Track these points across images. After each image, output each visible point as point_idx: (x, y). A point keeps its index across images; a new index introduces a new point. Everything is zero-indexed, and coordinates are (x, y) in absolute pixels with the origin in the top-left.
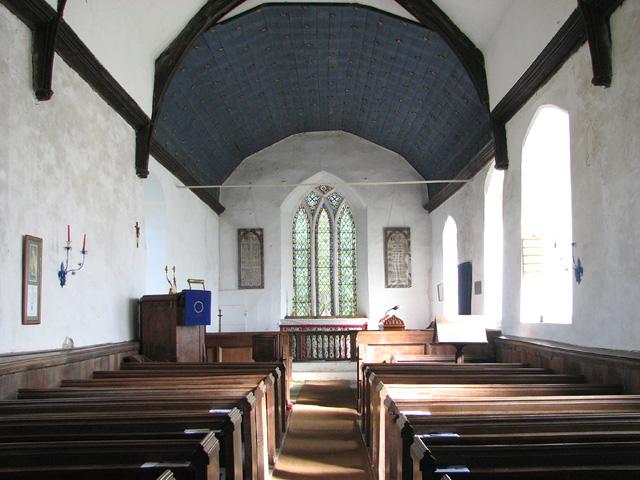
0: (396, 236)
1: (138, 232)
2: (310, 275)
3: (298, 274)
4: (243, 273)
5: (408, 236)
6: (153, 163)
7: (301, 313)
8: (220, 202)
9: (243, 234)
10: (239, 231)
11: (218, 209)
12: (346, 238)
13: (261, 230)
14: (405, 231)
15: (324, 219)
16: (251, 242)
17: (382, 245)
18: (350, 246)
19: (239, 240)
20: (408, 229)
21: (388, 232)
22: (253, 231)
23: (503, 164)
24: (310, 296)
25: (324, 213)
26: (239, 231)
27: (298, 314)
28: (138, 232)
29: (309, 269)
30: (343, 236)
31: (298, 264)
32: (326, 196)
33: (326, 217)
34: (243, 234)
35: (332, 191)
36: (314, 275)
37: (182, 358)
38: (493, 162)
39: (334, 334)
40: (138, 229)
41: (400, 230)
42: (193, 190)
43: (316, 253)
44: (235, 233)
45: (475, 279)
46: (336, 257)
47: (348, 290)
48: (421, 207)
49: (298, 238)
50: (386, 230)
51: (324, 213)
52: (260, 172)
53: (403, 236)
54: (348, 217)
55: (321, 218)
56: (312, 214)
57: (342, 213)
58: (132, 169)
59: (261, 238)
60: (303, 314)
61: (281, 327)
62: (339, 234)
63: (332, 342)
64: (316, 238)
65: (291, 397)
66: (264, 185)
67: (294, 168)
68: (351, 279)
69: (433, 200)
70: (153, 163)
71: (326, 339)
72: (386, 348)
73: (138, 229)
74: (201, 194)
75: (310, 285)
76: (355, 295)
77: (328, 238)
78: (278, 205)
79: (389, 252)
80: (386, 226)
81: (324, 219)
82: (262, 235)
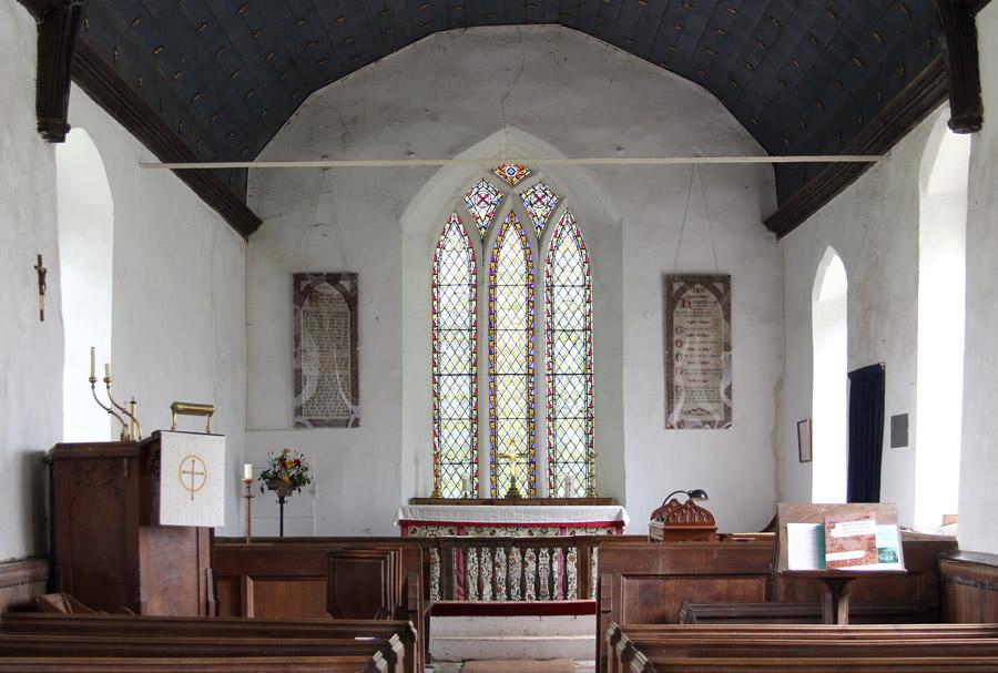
0: (694, 295)
1: (42, 282)
3: (444, 390)
6: (79, 101)
7: (451, 490)
11: (245, 222)
12: (570, 305)
14: (716, 285)
15: (511, 253)
16: (327, 305)
18: (577, 322)
20: (726, 279)
21: (676, 287)
22: (334, 279)
23: (968, 118)
24: (474, 447)
25: (512, 237)
27: (446, 494)
28: (42, 282)
30: (560, 296)
31: (447, 364)
32: (517, 190)
33: (518, 247)
34: (304, 288)
37: (154, 605)
38: (944, 112)
39: (537, 544)
40: (42, 275)
42: (179, 173)
45: (891, 409)
47: (570, 432)
49: (444, 300)
50: (669, 280)
51: (512, 237)
52: (348, 132)
54: (573, 248)
55: (506, 248)
57: (558, 236)
58: (29, 119)
59: (352, 301)
60: (457, 494)
61: (404, 524)
63: (532, 566)
66: (363, 161)
67: (434, 118)
68: (581, 404)
69: (790, 206)
70: (79, 101)
72: (670, 583)
73: (42, 275)
74: (202, 184)
75: (475, 420)
80: (669, 269)
81: (511, 253)
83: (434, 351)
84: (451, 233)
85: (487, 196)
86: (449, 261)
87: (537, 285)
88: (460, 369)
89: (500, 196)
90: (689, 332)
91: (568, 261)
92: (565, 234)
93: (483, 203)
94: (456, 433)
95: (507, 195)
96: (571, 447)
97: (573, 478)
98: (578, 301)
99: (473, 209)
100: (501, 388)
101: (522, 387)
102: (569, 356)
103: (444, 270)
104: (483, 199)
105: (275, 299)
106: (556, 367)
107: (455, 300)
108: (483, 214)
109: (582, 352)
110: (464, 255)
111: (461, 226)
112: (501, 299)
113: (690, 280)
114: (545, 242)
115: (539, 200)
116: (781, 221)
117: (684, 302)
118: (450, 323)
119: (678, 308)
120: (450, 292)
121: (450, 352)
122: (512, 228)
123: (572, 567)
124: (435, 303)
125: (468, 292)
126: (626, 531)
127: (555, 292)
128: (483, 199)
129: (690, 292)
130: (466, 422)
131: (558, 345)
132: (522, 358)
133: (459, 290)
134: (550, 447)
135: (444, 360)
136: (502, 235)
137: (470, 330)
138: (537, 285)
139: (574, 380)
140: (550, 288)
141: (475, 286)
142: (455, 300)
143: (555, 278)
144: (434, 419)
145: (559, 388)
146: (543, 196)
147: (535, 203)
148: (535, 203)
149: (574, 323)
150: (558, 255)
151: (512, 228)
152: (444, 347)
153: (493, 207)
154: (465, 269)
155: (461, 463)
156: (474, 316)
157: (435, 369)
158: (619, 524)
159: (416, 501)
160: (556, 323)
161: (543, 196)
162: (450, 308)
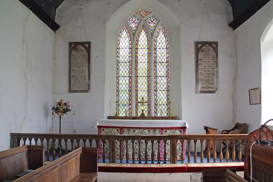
0: (205, 48)
2: (130, 83)
3: (121, 81)
4: (72, 80)
5: (216, 50)
7: (122, 114)
8: (56, 21)
9: (73, 46)
10: (71, 44)
11: (54, 27)
12: (162, 54)
13: (89, 43)
14: (214, 45)
15: (143, 38)
17: (193, 56)
18: (164, 59)
19: (70, 52)
20: (216, 43)
22: (83, 44)
25: (143, 33)
26: (71, 44)
27: (121, 115)
29: (130, 77)
30: (159, 52)
34: (73, 46)
35: (151, 15)
36: (134, 82)
41: (210, 44)
43: (136, 65)
44: (68, 45)
46: (153, 67)
48: (227, 24)
49: (121, 53)
50: (197, 43)
51: (143, 33)
53: (212, 49)
54: (163, 36)
56: (134, 37)
59: (89, 51)
61: (99, 127)
62: (156, 91)
64: (137, 82)
65: (113, 162)
71: (150, 144)
75: (130, 91)
76: (168, 99)
77: (146, 53)
78: (105, 22)
79: (199, 62)
80: (197, 40)
81: (143, 38)
82: (89, 46)
83: (117, 69)
84: (123, 32)
85: (135, 21)
86: (123, 41)
87: (151, 48)
88: (126, 75)
89: (139, 21)
90: (204, 61)
91: (161, 40)
92: (160, 32)
93: (134, 23)
94: (124, 95)
95: (141, 20)
96: (162, 100)
97: (162, 111)
98: (165, 53)
99: (131, 25)
100: (139, 81)
101: (146, 81)
102: (162, 71)
103: (121, 44)
104: (134, 22)
105: (64, 51)
106: (157, 74)
107: (124, 53)
108: (134, 27)
109: (166, 69)
110: (127, 39)
111: (127, 30)
112: (139, 53)
113: (204, 43)
114: (154, 34)
115: (152, 21)
116: (234, 25)
117: (202, 50)
118: (123, 60)
119: (200, 53)
120: (123, 50)
121: (122, 69)
122: (143, 30)
123: (168, 147)
124: (118, 54)
125: (128, 50)
126: (187, 133)
127: (157, 50)
128: (134, 22)
129: (204, 48)
130: (127, 92)
131: (158, 67)
132: (146, 71)
133: (126, 50)
134: (155, 100)
135: (121, 72)
136: (140, 33)
137: (129, 62)
138: (151, 48)
139: (163, 78)
140: (155, 49)
141: (131, 48)
142: (124, 53)
143: (157, 46)
144: (117, 91)
145: (158, 81)
146: (153, 21)
147: (151, 22)
148: (151, 22)
149: (163, 60)
150: (158, 39)
151: (143, 30)
152: (120, 67)
153: (137, 24)
154: (128, 43)
155: (126, 105)
156: (131, 58)
157: (118, 75)
158: (184, 128)
159: (110, 118)
160: (157, 60)
161: (153, 21)
162: (123, 55)
